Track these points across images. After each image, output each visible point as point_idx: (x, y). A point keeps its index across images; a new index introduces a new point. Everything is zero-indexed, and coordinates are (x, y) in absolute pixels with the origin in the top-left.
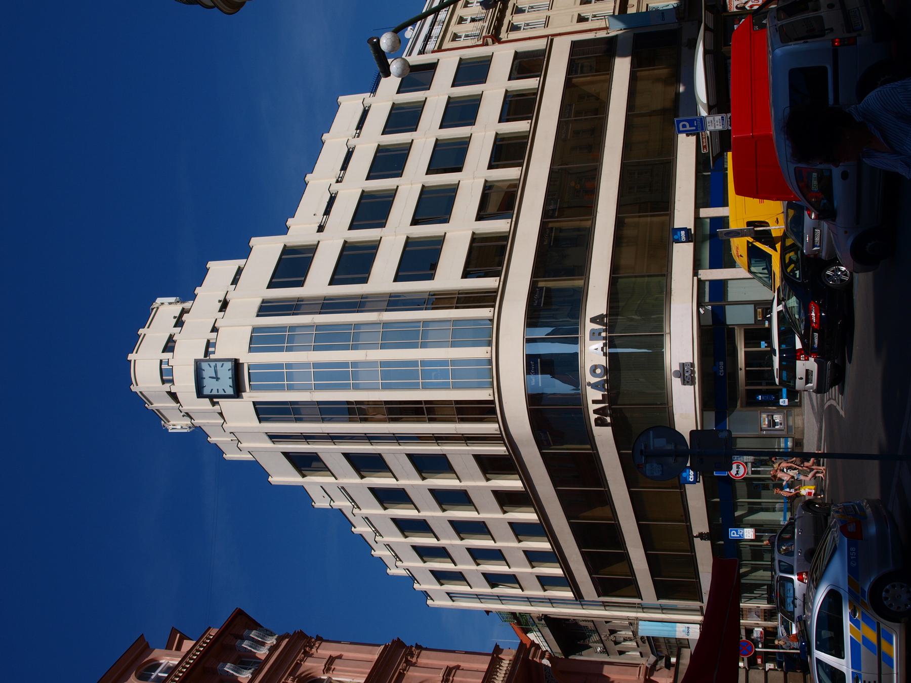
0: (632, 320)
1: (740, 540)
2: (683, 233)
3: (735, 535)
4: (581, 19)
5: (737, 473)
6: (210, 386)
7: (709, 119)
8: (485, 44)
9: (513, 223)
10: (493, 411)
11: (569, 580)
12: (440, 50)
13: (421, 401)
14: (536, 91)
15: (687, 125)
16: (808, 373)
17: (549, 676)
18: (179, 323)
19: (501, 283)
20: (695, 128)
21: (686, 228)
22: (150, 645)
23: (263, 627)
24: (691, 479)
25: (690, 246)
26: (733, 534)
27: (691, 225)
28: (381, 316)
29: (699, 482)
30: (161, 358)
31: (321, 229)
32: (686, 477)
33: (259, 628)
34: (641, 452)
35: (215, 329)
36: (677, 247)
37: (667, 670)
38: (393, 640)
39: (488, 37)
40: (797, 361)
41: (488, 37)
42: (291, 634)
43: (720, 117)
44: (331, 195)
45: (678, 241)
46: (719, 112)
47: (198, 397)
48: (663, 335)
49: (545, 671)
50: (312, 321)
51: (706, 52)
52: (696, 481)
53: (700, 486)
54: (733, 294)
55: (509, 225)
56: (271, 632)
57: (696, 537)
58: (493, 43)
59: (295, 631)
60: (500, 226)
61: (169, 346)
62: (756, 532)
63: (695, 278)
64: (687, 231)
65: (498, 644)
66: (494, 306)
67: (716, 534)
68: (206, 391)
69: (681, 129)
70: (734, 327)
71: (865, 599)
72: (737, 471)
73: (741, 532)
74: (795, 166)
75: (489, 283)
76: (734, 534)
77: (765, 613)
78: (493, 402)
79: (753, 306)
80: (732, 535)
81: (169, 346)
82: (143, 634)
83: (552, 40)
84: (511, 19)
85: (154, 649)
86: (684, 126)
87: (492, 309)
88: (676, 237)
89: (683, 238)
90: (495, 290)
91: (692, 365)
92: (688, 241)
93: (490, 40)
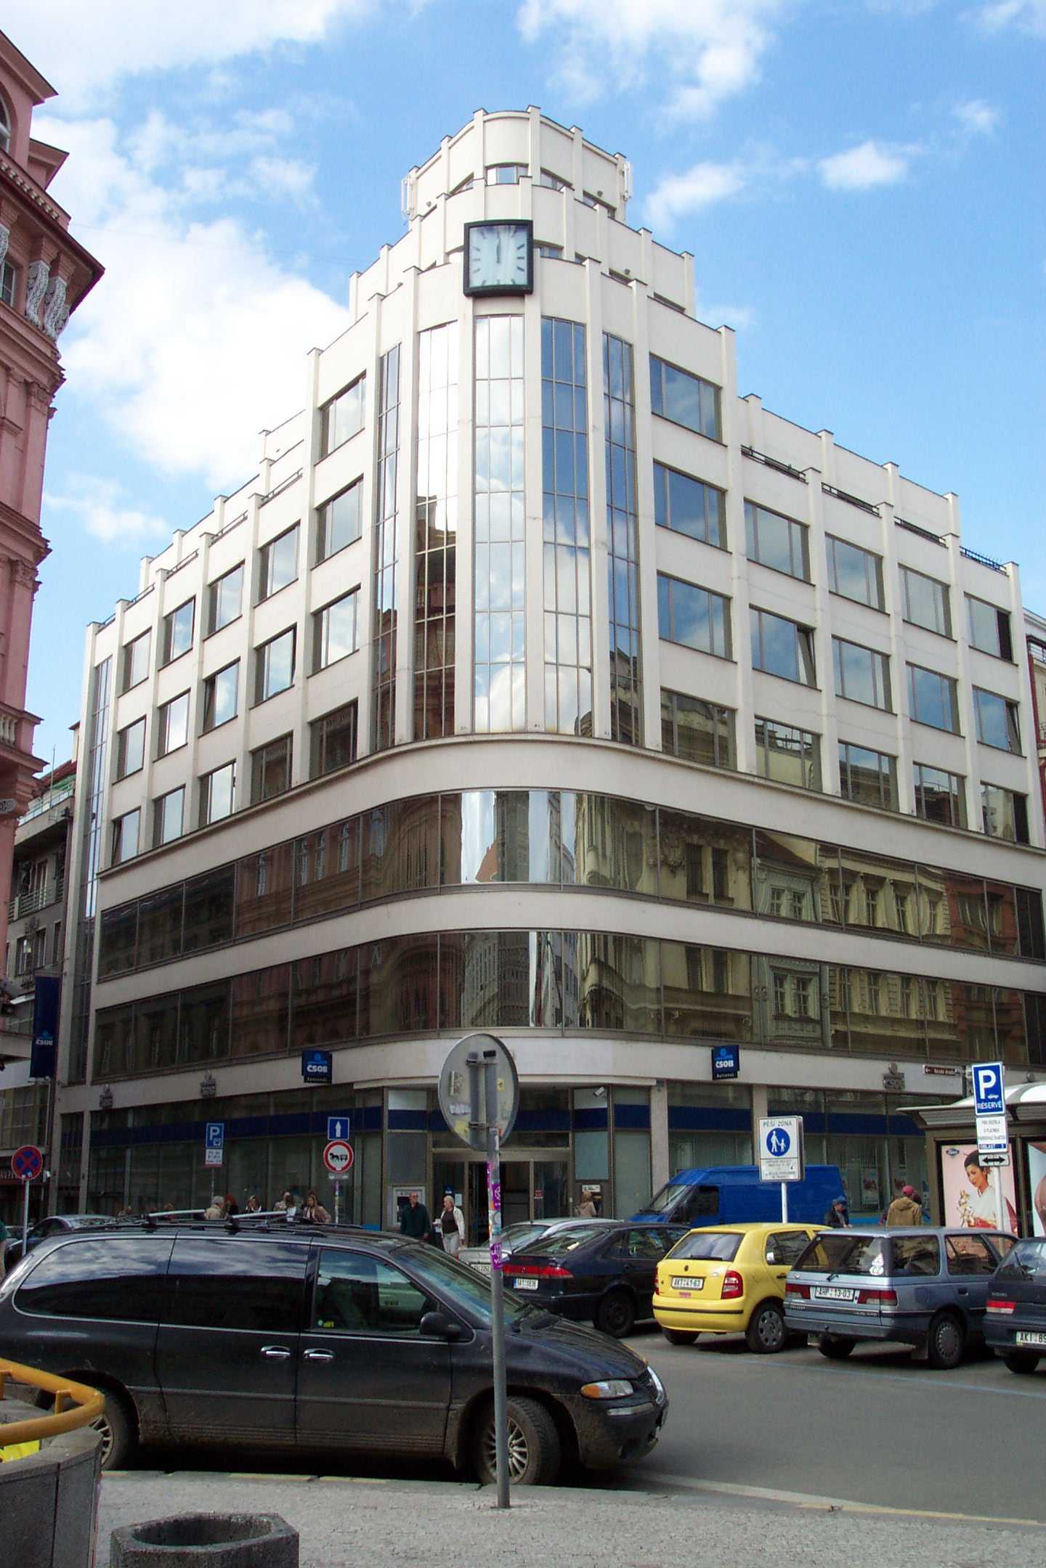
2: (731, 1064)
3: (212, 1134)
14: (962, 824)
15: (991, 1084)
18: (592, 199)
21: (738, 1069)
22: (37, 106)
23: (70, 314)
27: (742, 1078)
29: (306, 1081)
31: (747, 453)
33: (69, 307)
35: (580, 259)
38: (49, 541)
44: (802, 473)
45: (715, 1056)
47: (465, 224)
53: (298, 1082)
54: (628, 1144)
56: (61, 329)
57: (895, 1067)
59: (64, 370)
60: (746, 754)
61: (556, 181)
62: (215, 1168)
63: (654, 1083)
64: (734, 1071)
65: (42, 722)
67: (212, 1105)
70: (571, 1145)
72: (337, 1157)
73: (217, 1143)
75: (652, 734)
76: (215, 1131)
78: (450, 732)
80: (212, 1128)
81: (556, 181)
82: (57, 94)
87: (610, 737)
88: (723, 1052)
89: (721, 1064)
90: (640, 742)
92: (715, 1071)
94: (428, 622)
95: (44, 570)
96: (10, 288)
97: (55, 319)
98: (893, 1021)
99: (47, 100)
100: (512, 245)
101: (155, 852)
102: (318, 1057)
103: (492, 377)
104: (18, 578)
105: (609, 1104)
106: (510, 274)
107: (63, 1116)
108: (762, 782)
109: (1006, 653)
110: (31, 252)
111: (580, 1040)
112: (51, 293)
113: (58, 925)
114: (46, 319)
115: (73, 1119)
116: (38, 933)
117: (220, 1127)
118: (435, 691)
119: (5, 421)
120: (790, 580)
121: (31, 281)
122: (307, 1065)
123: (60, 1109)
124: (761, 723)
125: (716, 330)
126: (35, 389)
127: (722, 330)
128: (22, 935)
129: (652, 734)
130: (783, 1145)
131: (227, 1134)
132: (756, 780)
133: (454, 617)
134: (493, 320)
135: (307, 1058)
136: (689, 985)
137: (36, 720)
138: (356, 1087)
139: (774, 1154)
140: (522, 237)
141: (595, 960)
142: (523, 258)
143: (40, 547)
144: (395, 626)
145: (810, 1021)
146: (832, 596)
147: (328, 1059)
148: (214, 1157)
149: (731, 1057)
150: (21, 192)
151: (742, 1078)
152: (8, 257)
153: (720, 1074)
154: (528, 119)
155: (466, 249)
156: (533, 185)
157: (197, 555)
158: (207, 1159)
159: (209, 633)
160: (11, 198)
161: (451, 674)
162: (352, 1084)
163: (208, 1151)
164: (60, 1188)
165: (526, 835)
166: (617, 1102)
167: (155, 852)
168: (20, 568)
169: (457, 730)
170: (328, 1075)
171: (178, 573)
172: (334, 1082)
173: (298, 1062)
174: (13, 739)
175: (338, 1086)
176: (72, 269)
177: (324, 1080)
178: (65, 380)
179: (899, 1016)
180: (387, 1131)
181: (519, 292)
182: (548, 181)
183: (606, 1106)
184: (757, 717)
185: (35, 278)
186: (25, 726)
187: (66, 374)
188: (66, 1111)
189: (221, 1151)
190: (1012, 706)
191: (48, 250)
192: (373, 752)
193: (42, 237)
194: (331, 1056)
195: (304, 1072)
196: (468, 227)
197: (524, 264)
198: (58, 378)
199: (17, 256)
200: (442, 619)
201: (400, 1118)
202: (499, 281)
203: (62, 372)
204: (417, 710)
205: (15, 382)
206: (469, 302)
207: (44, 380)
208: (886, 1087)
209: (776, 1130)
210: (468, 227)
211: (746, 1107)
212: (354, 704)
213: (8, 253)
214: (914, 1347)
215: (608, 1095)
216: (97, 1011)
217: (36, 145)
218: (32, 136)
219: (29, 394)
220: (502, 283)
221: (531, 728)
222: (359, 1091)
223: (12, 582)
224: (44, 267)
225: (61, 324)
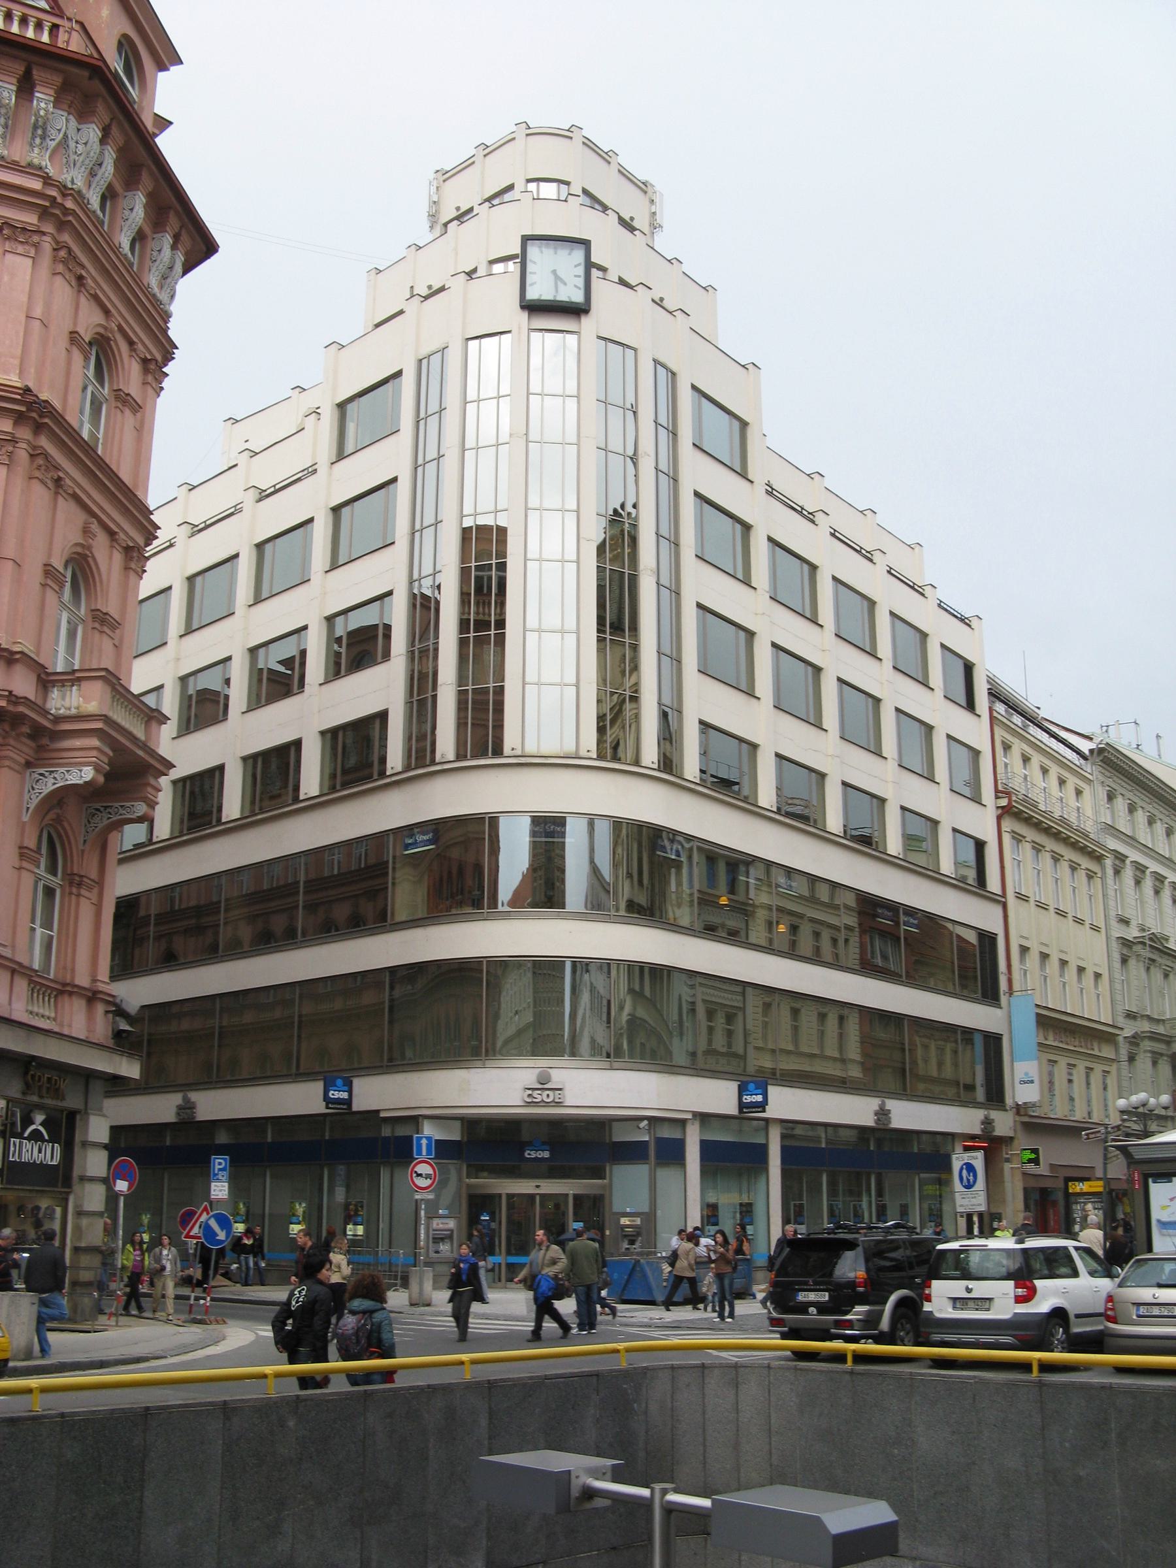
0: (621, 1008)
1: (207, 1176)
2: (759, 1098)
3: (217, 1167)
4: (1024, 950)
5: (419, 1175)
8: (998, 793)
10: (481, 752)
12: (992, 719)
16: (985, 1302)
17: (110, 813)
24: (334, 1094)
25: (731, 1108)
26: (219, 1163)
28: (649, 572)
29: (327, 1108)
30: (572, 185)
31: (771, 492)
36: (731, 1088)
39: (1010, 800)
40: (1013, 1282)
41: (1010, 800)
45: (742, 1090)
47: (522, 236)
49: (122, 806)
54: (666, 1176)
57: (883, 1103)
58: (998, 807)
59: (177, 348)
63: (689, 1116)
64: (762, 1106)
68: (533, 250)
74: (349, 1288)
76: (220, 1164)
79: (646, 1210)
83: (998, 902)
84: (1027, 839)
88: (751, 1086)
89: (748, 1099)
91: (558, 1104)
92: (742, 1106)
93: (1004, 802)
99: (172, 68)
100: (570, 262)
101: (137, 852)
102: (339, 1082)
103: (546, 392)
105: (650, 1137)
109: (970, 705)
110: (156, 223)
111: (647, 1073)
118: (480, 705)
122: (329, 1090)
125: (743, 366)
127: (750, 367)
129: (691, 768)
130: (971, 1178)
131: (233, 1162)
134: (547, 335)
138: (382, 1115)
139: (966, 1187)
140: (579, 255)
141: (631, 991)
142: (579, 276)
144: (437, 637)
145: (735, 1055)
148: (220, 1190)
149: (760, 1091)
153: (333, 1103)
155: (522, 259)
158: (212, 1193)
160: (153, 167)
161: (500, 691)
162: (378, 1111)
163: (213, 1184)
165: (563, 857)
166: (659, 1135)
167: (137, 852)
169: (507, 750)
170: (349, 1102)
172: (355, 1108)
173: (319, 1086)
177: (345, 1107)
178: (173, 358)
181: (576, 311)
182: (588, 201)
183: (646, 1138)
189: (226, 1184)
190: (976, 753)
191: (173, 222)
192: (407, 768)
193: (170, 208)
194: (351, 1082)
195: (326, 1098)
196: (526, 239)
203: (175, 351)
204: (461, 724)
208: (876, 1123)
209: (965, 1164)
210: (526, 239)
211: (763, 1142)
212: (383, 716)
220: (543, 298)
222: (386, 1119)
224: (167, 240)
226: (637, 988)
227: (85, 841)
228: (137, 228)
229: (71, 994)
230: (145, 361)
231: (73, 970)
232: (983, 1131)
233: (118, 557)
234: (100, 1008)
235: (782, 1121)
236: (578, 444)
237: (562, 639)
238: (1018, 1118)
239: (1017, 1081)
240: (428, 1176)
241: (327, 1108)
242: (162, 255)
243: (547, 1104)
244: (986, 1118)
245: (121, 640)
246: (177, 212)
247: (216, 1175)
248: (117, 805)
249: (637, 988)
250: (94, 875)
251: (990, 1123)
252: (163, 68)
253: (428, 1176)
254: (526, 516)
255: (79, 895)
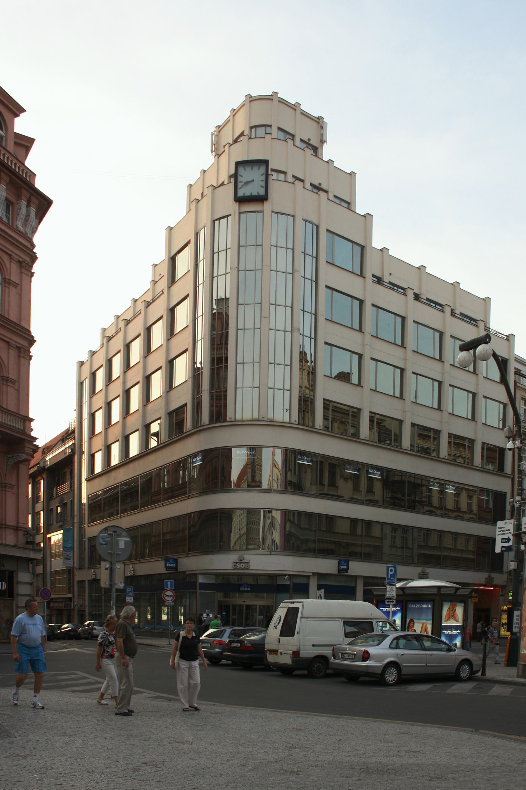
2: (345, 567)
3: (128, 591)
5: (167, 596)
6: (246, 174)
7: (394, 588)
9: (365, 442)
10: (218, 420)
11: (108, 469)
13: (227, 363)
15: (392, 573)
19: (317, 431)
20: (389, 577)
27: (350, 572)
29: (166, 570)
32: (169, 561)
33: (38, 221)
34: (115, 532)
37: (25, 542)
42: (35, 250)
43: (394, 595)
46: (397, 595)
48: (315, 553)
50: (296, 270)
51: (439, 588)
52: (167, 568)
53: (163, 570)
55: (364, 438)
60: (365, 430)
63: (311, 574)
64: (347, 570)
66: (299, 424)
68: (241, 170)
69: (390, 568)
71: (87, 678)
72: (168, 596)
75: (319, 421)
76: (129, 589)
77: (83, 611)
78: (225, 421)
80: (128, 588)
85: (15, 133)
86: (391, 571)
87: (297, 423)
88: (343, 562)
89: (341, 567)
92: (339, 570)
94: (217, 368)
95: (33, 350)
96: (9, 215)
97: (32, 228)
98: (462, 551)
102: (171, 560)
104: (22, 355)
106: (256, 189)
107: (78, 582)
108: (371, 443)
112: (28, 215)
113: (71, 501)
114: (27, 229)
115: (81, 583)
116: (64, 503)
117: (131, 588)
119: (11, 281)
120: (393, 346)
121: (18, 211)
123: (77, 578)
124: (373, 415)
126: (24, 264)
128: (58, 505)
132: (368, 442)
133: (227, 365)
135: (167, 560)
136: (351, 531)
137: (32, 420)
138: (187, 573)
143: (31, 340)
146: (414, 353)
147: (176, 561)
149: (345, 564)
150: (8, 166)
151: (350, 572)
152: (7, 199)
153: (341, 571)
154: (272, 99)
156: (272, 138)
157: (121, 330)
158: (127, 600)
159: (127, 368)
162: (185, 572)
164: (78, 611)
168: (22, 350)
169: (228, 419)
170: (176, 568)
171: (117, 336)
174: (22, 428)
175: (180, 572)
176: (37, 202)
179: (464, 548)
180: (198, 591)
182: (281, 135)
183: (289, 583)
184: (371, 412)
185: (20, 209)
186: (27, 422)
187: (38, 255)
188: (78, 580)
189: (132, 597)
197: (263, 184)
198: (34, 258)
199: (10, 198)
200: (222, 366)
201: (204, 586)
202: (251, 193)
205: (14, 262)
206: (237, 205)
207: (28, 259)
211: (353, 585)
213: (6, 198)
214: (224, 653)
215: (290, 578)
216: (88, 538)
217: (18, 136)
218: (15, 131)
219: (21, 267)
221: (261, 418)
223: (19, 356)
224: (24, 203)
225: (34, 231)
226: (292, 519)
227: (6, 470)
228: (5, 198)
229: (5, 528)
230: (20, 262)
231: (5, 520)
232: (486, 582)
233: (13, 353)
234: (21, 533)
235: (365, 577)
236: (292, 274)
237: (253, 366)
238: (509, 577)
239: (509, 560)
240: (171, 596)
241: (166, 570)
242: (21, 211)
243: (242, 569)
244: (489, 576)
245: (19, 386)
246: (25, 189)
247: (127, 594)
248: (16, 455)
249: (292, 519)
250: (14, 482)
251: (492, 579)
252: (17, 116)
253: (171, 596)
254: (238, 308)
255: (6, 491)
